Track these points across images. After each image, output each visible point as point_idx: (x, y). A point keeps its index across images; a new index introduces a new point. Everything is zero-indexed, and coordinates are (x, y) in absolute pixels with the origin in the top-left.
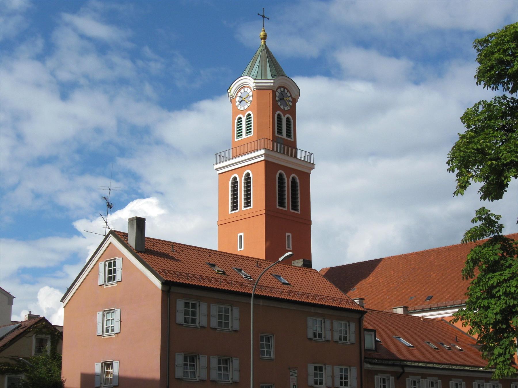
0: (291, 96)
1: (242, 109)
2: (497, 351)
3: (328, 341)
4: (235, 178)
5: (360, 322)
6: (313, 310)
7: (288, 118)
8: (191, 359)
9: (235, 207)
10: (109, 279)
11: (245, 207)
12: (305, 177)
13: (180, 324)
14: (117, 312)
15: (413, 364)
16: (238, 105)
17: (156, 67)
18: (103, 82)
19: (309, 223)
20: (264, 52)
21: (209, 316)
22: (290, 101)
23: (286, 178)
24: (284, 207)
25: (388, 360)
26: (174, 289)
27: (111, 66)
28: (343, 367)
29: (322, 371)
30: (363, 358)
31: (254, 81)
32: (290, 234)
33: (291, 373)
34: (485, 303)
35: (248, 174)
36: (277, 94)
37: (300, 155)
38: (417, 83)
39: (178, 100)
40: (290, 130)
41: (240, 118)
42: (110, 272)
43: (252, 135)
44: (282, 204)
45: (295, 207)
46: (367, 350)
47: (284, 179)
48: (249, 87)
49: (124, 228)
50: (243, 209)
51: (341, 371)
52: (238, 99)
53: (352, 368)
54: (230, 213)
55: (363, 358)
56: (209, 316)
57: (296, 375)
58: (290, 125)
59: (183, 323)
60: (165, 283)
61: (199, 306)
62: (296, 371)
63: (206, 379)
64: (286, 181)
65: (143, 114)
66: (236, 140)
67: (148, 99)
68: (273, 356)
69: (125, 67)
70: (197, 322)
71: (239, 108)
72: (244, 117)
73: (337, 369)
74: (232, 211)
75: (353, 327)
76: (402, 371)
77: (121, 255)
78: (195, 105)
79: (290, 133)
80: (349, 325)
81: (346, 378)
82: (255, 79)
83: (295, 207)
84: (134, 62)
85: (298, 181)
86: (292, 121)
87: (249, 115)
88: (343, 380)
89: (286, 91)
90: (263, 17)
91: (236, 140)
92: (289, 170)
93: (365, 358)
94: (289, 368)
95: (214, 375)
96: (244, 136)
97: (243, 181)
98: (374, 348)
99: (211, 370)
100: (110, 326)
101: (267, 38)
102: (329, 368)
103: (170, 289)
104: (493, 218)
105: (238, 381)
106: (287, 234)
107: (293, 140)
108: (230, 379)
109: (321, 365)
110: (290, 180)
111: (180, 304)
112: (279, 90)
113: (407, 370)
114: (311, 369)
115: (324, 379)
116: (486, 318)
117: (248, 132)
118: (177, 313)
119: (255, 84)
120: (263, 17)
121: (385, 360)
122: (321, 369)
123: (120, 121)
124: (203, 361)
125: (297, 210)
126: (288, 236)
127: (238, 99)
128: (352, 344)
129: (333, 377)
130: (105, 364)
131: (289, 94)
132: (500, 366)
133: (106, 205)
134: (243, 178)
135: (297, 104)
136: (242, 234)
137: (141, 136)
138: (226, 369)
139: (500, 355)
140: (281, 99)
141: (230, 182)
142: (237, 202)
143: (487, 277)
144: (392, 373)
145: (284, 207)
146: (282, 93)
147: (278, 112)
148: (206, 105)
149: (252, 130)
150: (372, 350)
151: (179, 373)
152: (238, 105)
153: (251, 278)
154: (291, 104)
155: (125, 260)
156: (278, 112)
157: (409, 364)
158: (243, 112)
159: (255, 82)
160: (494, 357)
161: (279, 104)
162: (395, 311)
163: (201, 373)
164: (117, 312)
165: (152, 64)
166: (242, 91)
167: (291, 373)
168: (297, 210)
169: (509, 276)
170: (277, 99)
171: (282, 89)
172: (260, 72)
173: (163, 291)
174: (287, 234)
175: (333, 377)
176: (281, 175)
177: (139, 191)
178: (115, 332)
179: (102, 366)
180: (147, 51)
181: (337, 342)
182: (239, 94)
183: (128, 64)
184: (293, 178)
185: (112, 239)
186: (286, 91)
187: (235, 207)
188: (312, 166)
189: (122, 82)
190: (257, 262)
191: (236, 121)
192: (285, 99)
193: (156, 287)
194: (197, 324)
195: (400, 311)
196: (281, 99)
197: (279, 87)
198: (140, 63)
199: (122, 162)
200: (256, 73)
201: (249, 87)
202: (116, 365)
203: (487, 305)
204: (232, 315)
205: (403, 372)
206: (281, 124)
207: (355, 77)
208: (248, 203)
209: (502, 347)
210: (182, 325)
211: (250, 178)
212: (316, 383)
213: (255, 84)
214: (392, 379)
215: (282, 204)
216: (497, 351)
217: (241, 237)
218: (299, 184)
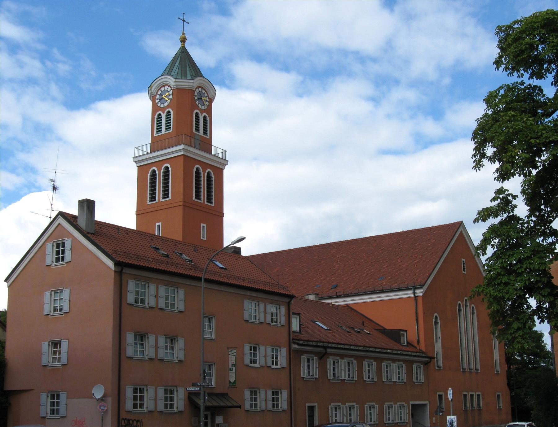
0: (208, 96)
1: (162, 106)
2: (515, 326)
3: (261, 323)
4: (154, 171)
5: (289, 305)
6: (249, 293)
7: (205, 117)
8: (141, 337)
9: (153, 198)
10: (57, 260)
11: (163, 198)
12: (219, 172)
13: (130, 304)
14: (66, 292)
15: (333, 346)
16: (158, 103)
17: (64, 68)
18: (11, 80)
19: (222, 215)
20: (183, 54)
21: (157, 296)
22: (206, 101)
23: (202, 173)
24: (200, 199)
25: (313, 341)
26: (126, 270)
27: (21, 65)
28: (274, 348)
29: (256, 351)
30: (291, 339)
31: (174, 80)
32: (205, 225)
33: (230, 353)
34: (505, 279)
35: (167, 168)
36: (196, 94)
37: (214, 151)
38: (300, 96)
39: (79, 99)
40: (206, 128)
41: (160, 115)
42: (58, 253)
43: (172, 131)
44: (198, 196)
45: (209, 200)
46: (294, 332)
47: (200, 173)
48: (169, 86)
49: (74, 211)
50: (161, 200)
51: (273, 352)
52: (158, 97)
53: (282, 348)
54: (148, 203)
55: (291, 339)
56: (157, 296)
57: (235, 354)
58: (207, 123)
59: (134, 303)
60: (117, 264)
61: (149, 287)
62: (235, 351)
63: (154, 357)
64: (202, 175)
65: (48, 112)
66: (155, 135)
67: (54, 99)
68: (213, 337)
69: (34, 67)
70: (146, 302)
71: (159, 105)
72: (164, 113)
73: (269, 349)
74: (150, 201)
75: (283, 310)
76: (324, 352)
77: (70, 235)
78: (93, 106)
79: (206, 131)
80: (280, 309)
81: (277, 358)
82: (176, 79)
83: (209, 200)
84: (43, 63)
85: (213, 175)
86: (208, 119)
87: (169, 112)
88: (274, 360)
89: (204, 91)
90: (184, 21)
91: (155, 135)
92: (205, 165)
93: (293, 339)
94: (228, 348)
95: (161, 354)
96: (163, 131)
97: (162, 174)
98: (298, 330)
99: (159, 349)
100: (58, 305)
101: (187, 41)
102: (262, 348)
103: (122, 270)
104: (510, 198)
105: (183, 360)
106: (202, 225)
107: (209, 137)
108: (175, 358)
109: (255, 346)
110: (206, 174)
111: (131, 285)
112: (197, 91)
113: (328, 350)
114: (247, 348)
115: (258, 358)
116: (507, 293)
117: (168, 128)
118: (128, 294)
119: (175, 84)
120: (184, 21)
121: (306, 341)
122: (255, 349)
123: (26, 119)
124: (151, 340)
125: (211, 203)
126: (203, 227)
127: (158, 97)
128: (282, 326)
129: (265, 357)
130: (52, 343)
131: (206, 95)
132: (520, 339)
133: (51, 188)
134: (162, 171)
135: (213, 104)
136: (160, 224)
137: (44, 132)
138: (172, 348)
139: (519, 329)
140: (200, 99)
141: (149, 175)
142: (155, 193)
143: (508, 254)
144: (316, 354)
145: (200, 199)
146: (200, 93)
147: (196, 111)
148: (103, 105)
149: (172, 126)
150: (297, 332)
151: (130, 351)
152: (158, 103)
153: (191, 261)
154: (208, 103)
155: (74, 239)
156: (196, 111)
157: (330, 345)
158: (163, 110)
159: (175, 82)
160: (512, 331)
161: (197, 103)
162: (307, 297)
163: (149, 352)
164: (66, 292)
165: (60, 66)
166: (163, 89)
167: (230, 353)
168: (211, 203)
169: (531, 253)
170: (196, 98)
171: (200, 89)
172: (180, 71)
173: (115, 271)
174: (202, 225)
175: (265, 357)
176: (197, 169)
177: (37, 185)
178: (63, 311)
179: (49, 345)
180: (56, 52)
181: (269, 324)
182: (159, 92)
183: (37, 64)
184: (209, 173)
185: (61, 220)
186: (204, 91)
187: (153, 198)
188: (225, 162)
189: (31, 81)
190: (195, 247)
191: (156, 117)
192: (203, 98)
193: (109, 267)
194: (146, 305)
195: (312, 297)
196: (199, 99)
197: (198, 87)
198: (49, 64)
199: (22, 156)
200: (176, 73)
201: (169, 86)
202: (65, 345)
203: (507, 281)
204: (178, 296)
205: (326, 353)
206: (199, 122)
207: (248, 88)
208: (166, 195)
209: (521, 321)
210: (133, 305)
211: (169, 171)
212: (251, 362)
213: (175, 84)
214: (316, 358)
215: (198, 196)
216: (515, 326)
217: (159, 226)
218: (213, 179)
